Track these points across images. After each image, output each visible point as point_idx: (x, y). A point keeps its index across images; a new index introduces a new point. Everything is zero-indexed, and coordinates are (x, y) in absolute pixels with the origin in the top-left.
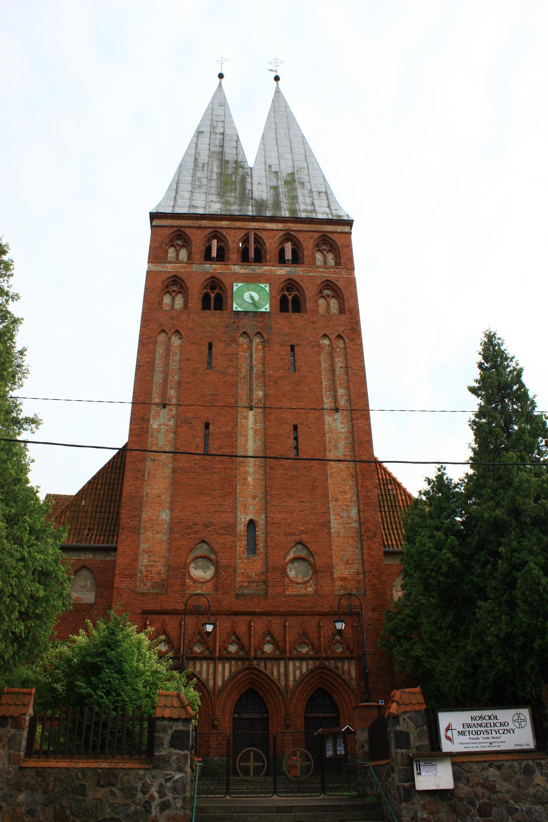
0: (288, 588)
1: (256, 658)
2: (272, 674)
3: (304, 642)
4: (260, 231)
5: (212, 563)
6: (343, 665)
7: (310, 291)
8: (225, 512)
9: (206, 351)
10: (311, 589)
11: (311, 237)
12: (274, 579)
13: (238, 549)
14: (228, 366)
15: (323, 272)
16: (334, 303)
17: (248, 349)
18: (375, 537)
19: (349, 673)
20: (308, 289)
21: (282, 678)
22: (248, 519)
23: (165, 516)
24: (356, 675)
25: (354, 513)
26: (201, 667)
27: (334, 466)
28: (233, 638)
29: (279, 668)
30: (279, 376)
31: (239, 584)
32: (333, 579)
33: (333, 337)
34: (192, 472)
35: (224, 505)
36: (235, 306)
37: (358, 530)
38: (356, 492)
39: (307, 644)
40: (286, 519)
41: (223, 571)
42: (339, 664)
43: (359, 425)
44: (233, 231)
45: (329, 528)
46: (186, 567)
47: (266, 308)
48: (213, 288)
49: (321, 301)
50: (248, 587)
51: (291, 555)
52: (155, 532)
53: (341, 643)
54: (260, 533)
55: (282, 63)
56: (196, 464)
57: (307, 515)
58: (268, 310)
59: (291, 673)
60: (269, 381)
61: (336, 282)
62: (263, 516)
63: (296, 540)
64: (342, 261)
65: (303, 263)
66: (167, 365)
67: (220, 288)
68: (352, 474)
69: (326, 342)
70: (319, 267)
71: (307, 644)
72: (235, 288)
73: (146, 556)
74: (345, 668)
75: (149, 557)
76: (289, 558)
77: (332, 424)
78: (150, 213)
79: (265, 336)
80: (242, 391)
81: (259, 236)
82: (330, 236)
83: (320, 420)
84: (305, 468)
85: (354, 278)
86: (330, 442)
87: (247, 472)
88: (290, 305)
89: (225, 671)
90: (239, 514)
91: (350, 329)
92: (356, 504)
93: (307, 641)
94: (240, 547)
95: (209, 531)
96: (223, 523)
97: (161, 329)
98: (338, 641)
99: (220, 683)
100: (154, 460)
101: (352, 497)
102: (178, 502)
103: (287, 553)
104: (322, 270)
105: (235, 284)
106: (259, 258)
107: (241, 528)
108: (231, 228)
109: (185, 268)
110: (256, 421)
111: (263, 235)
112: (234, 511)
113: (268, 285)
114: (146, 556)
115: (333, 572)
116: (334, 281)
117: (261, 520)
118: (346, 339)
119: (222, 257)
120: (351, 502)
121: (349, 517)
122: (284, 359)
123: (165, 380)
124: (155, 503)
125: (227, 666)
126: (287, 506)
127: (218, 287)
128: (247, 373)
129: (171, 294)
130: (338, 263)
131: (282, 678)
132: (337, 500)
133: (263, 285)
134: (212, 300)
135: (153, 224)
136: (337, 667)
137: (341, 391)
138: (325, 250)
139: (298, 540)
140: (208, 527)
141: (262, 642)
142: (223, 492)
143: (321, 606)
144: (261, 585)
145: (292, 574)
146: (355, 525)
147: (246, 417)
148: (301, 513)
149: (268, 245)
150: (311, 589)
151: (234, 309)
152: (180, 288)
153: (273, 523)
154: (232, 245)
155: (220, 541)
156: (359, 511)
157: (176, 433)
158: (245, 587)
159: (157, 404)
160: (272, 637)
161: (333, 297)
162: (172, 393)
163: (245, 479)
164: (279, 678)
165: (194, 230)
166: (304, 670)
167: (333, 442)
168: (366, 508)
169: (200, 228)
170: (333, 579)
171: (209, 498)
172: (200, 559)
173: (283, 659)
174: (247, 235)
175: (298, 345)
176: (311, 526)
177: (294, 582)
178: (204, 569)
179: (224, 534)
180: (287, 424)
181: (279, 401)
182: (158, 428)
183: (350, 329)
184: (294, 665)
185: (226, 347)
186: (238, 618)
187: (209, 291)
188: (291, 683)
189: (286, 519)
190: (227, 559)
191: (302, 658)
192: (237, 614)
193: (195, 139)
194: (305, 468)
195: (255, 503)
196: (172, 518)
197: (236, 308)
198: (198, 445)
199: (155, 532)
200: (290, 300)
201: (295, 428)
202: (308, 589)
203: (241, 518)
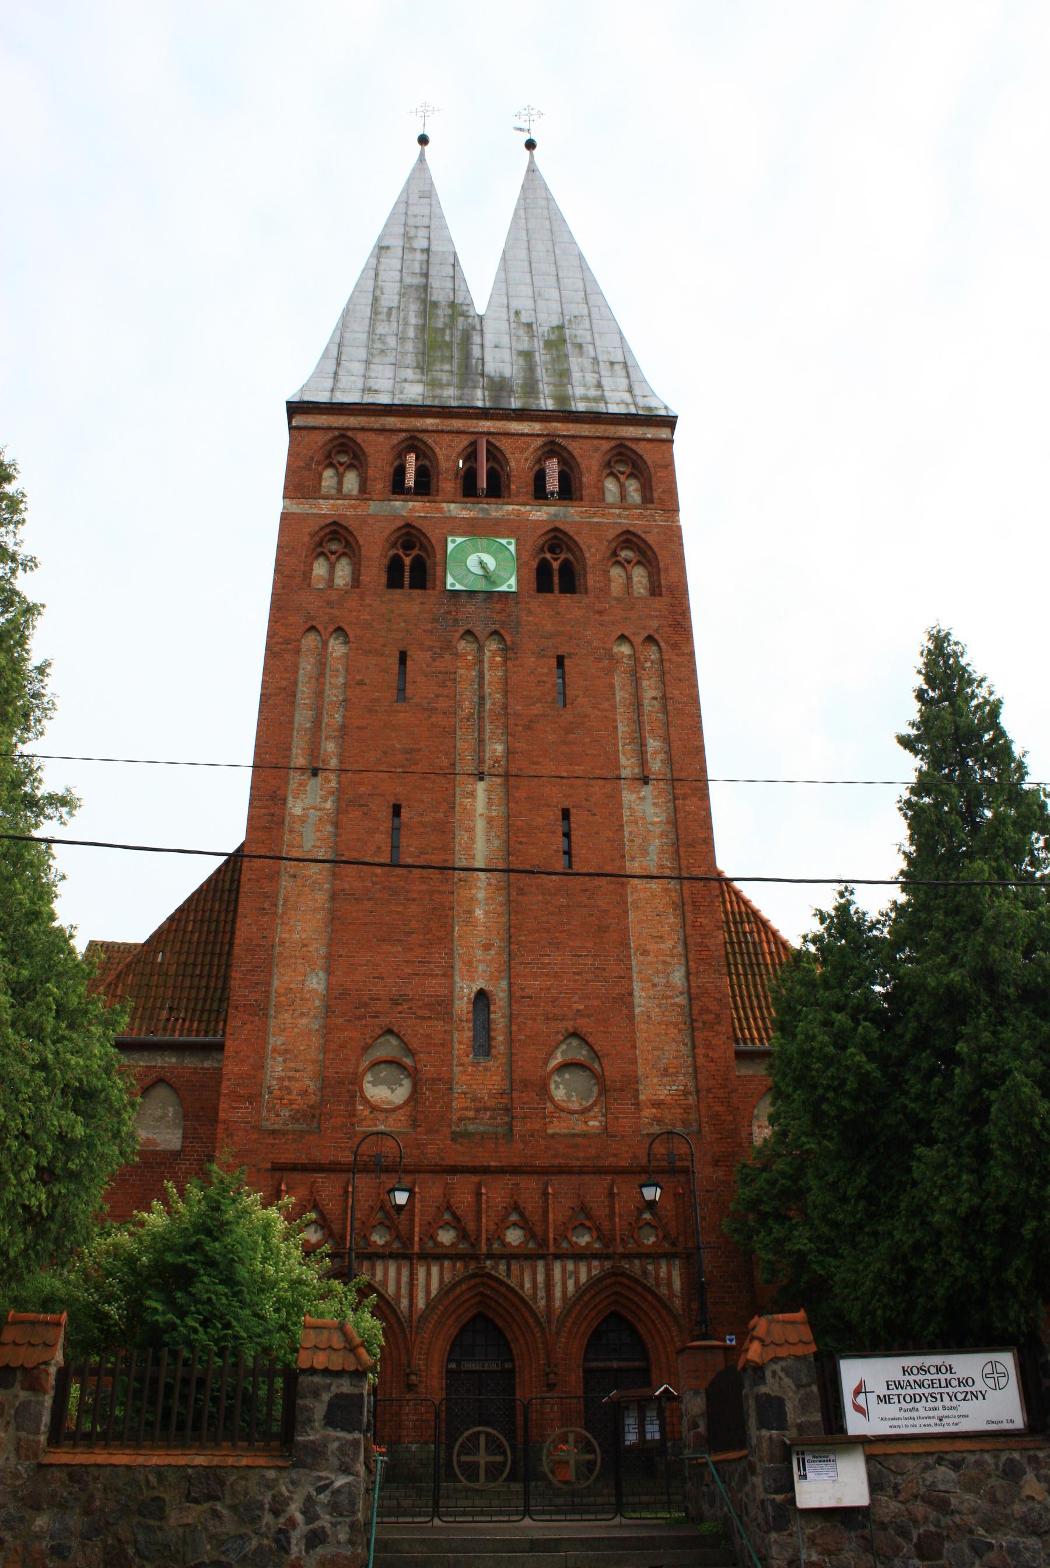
0: (552, 1122)
1: (490, 1256)
2: (522, 1286)
3: (582, 1225)
4: (498, 437)
5: (406, 1073)
6: (657, 1269)
7: (593, 552)
8: (431, 975)
9: (395, 668)
10: (597, 1124)
11: (596, 450)
12: (524, 1103)
13: (456, 1046)
14: (437, 696)
15: (619, 516)
18: (719, 1023)
19: (670, 1285)
20: (589, 547)
22: (474, 990)
23: (316, 983)
24: (682, 1289)
25: (678, 976)
28: (447, 1217)
29: (534, 1274)
31: (459, 1114)
36: (450, 580)
39: (589, 1228)
40: (548, 989)
41: (427, 1089)
42: (650, 1267)
43: (687, 808)
45: (631, 1006)
46: (357, 1081)
47: (510, 584)
48: (408, 546)
50: (475, 1119)
52: (297, 1013)
53: (654, 1227)
54: (498, 1015)
55: (541, 114)
57: (587, 981)
58: (514, 589)
60: (516, 725)
61: (643, 535)
62: (504, 984)
63: (567, 1030)
64: (655, 495)
65: (581, 499)
66: (319, 694)
67: (422, 547)
68: (674, 903)
70: (612, 506)
71: (589, 1228)
72: (450, 547)
73: (280, 1059)
75: (285, 1061)
76: (553, 1063)
77: (636, 808)
78: (288, 403)
79: (508, 638)
80: (464, 744)
81: (497, 448)
82: (634, 446)
83: (614, 799)
84: (586, 890)
85: (679, 528)
86: (632, 841)
87: (472, 899)
88: (556, 579)
89: (431, 1279)
90: (457, 979)
91: (670, 626)
92: (683, 961)
93: (588, 1223)
94: (460, 1043)
95: (400, 1013)
97: (309, 625)
99: (421, 1303)
100: (295, 876)
103: (550, 1055)
104: (617, 511)
105: (450, 539)
106: (497, 489)
107: (462, 1006)
111: (504, 444)
112: (448, 973)
113: (513, 541)
115: (637, 1090)
117: (500, 992)
118: (662, 644)
119: (425, 487)
120: (673, 956)
121: (668, 984)
123: (317, 722)
124: (296, 958)
126: (549, 964)
127: (418, 545)
128: (474, 708)
129: (327, 559)
130: (647, 499)
132: (645, 953)
133: (504, 541)
134: (407, 569)
136: (645, 1273)
138: (623, 473)
139: (571, 1030)
141: (503, 1225)
142: (427, 937)
143: (615, 1155)
145: (559, 1094)
146: (681, 1000)
147: (472, 794)
148: (577, 977)
150: (597, 1124)
151: (449, 587)
152: (345, 547)
153: (522, 997)
154: (444, 465)
155: (421, 1031)
157: (336, 825)
158: (469, 1119)
160: (522, 1215)
161: (639, 563)
162: (330, 747)
163: (470, 912)
164: (535, 1294)
165: (371, 436)
166: (583, 1278)
169: (382, 431)
170: (637, 1104)
171: (400, 949)
173: (542, 1257)
174: (474, 444)
175: (570, 655)
176: (596, 1003)
177: (563, 1110)
178: (391, 1084)
179: (430, 1018)
180: (549, 806)
181: (534, 763)
182: (303, 816)
183: (670, 626)
184: (564, 1269)
186: (456, 1178)
187: (401, 552)
188: (558, 1303)
189: (548, 989)
192: (453, 1170)
193: (374, 261)
194: (586, 890)
195: (490, 957)
196: (329, 987)
197: (453, 585)
199: (297, 1013)
200: (556, 568)
201: (566, 814)
202: (591, 1123)
203: (462, 988)
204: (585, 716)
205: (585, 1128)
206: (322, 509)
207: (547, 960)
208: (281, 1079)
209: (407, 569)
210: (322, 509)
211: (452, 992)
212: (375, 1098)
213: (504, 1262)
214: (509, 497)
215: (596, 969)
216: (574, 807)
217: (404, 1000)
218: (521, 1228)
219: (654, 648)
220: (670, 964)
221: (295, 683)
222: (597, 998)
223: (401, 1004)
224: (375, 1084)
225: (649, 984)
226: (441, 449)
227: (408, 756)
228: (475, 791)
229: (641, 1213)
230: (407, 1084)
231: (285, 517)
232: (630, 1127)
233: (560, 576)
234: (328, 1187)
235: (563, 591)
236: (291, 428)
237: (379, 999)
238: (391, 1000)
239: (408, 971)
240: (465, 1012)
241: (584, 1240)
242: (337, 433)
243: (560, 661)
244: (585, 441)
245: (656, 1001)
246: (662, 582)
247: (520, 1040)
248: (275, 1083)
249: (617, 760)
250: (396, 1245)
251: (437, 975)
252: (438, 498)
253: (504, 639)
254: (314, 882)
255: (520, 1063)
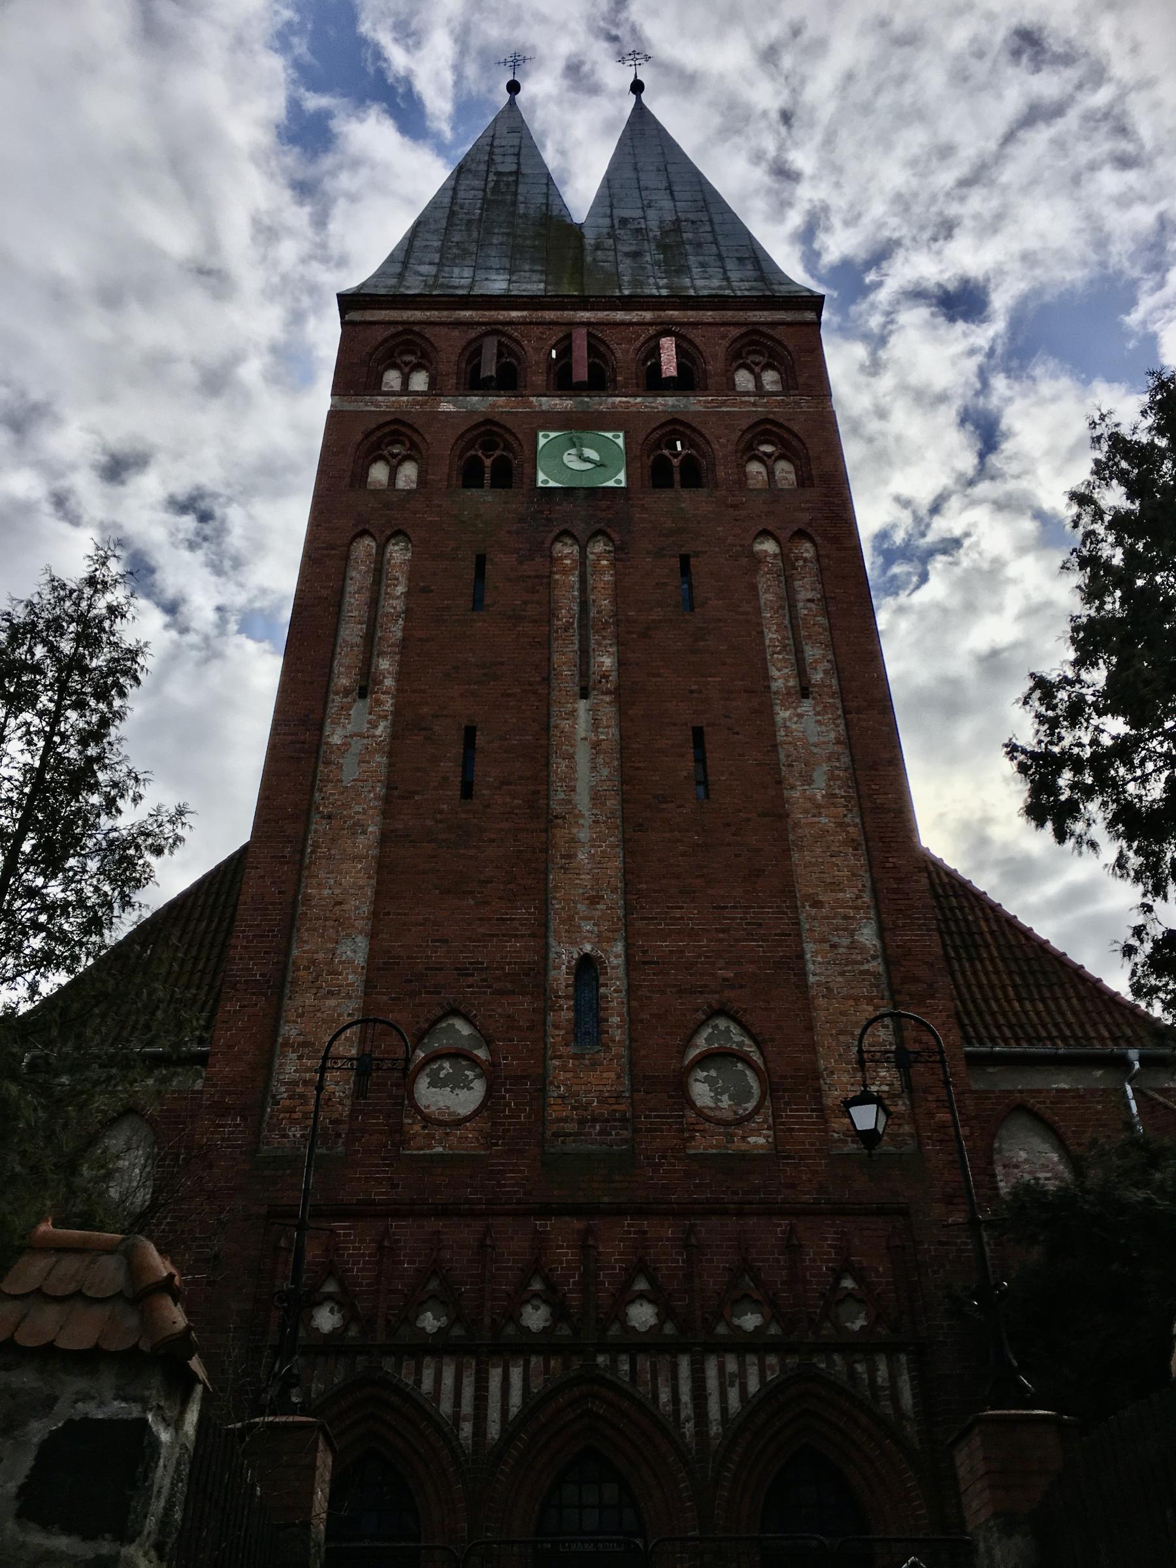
0: (693, 1138)
1: (602, 1348)
2: (656, 1397)
3: (747, 1297)
4: (600, 328)
5: (478, 1070)
6: (872, 1371)
7: (722, 445)
8: (516, 936)
9: (470, 575)
10: (762, 1141)
11: (723, 337)
12: (651, 1110)
13: (551, 1030)
14: (525, 603)
15: (754, 404)
16: (785, 471)
17: (575, 568)
18: (932, 997)
19: (895, 1398)
20: (718, 438)
21: (687, 1411)
22: (576, 956)
23: (355, 951)
24: (915, 1405)
25: (867, 936)
26: (438, 1380)
27: (803, 821)
28: (537, 1286)
29: (675, 1377)
30: (653, 621)
31: (554, 1128)
32: (821, 1110)
33: (785, 535)
34: (429, 842)
35: (512, 919)
36: (541, 476)
37: (884, 979)
38: (868, 884)
39: (756, 1302)
40: (682, 952)
41: (507, 1091)
42: (860, 1368)
43: (864, 724)
44: (537, 330)
45: (803, 974)
46: (407, 1080)
47: (619, 479)
48: (488, 447)
49: (755, 468)
50: (579, 1134)
51: (701, 1044)
52: (322, 992)
53: (860, 1301)
54: (614, 988)
56: (441, 821)
57: (737, 940)
58: (623, 485)
59: (717, 1392)
60: (629, 633)
61: (786, 423)
62: (619, 948)
63: (710, 1006)
64: (801, 380)
65: (706, 388)
66: (374, 603)
67: (508, 447)
68: (853, 840)
69: (769, 547)
70: (747, 394)
71: (756, 1302)
72: (542, 441)
73: (294, 1056)
74: (880, 1380)
75: (300, 1058)
76: (693, 1053)
77: (794, 726)
78: (338, 295)
79: (614, 536)
80: (564, 658)
81: (600, 340)
82: (770, 331)
83: (765, 712)
84: (728, 825)
85: (833, 414)
86: (791, 766)
87: (573, 840)
88: (677, 477)
89: (510, 1386)
90: (552, 942)
91: (827, 518)
92: (872, 913)
93: (756, 1295)
94: (557, 1027)
95: (469, 987)
96: (509, 964)
97: (360, 528)
98: (850, 1295)
99: (494, 1430)
100: (329, 817)
101: (858, 897)
102: (388, 914)
103: (688, 1042)
104: (752, 399)
105: (541, 434)
106: (599, 382)
107: (561, 977)
108: (531, 323)
109: (422, 404)
110: (596, 724)
111: (606, 335)
112: (541, 932)
113: (621, 434)
114: (294, 1056)
115: (819, 1090)
116: (781, 421)
117: (615, 956)
118: (818, 539)
119: (508, 380)
120: (857, 908)
121: (853, 945)
122: (665, 584)
123: (369, 639)
124: (326, 919)
125: (516, 1375)
126: (682, 918)
127: (502, 445)
128: (573, 617)
129: (388, 462)
130: (789, 384)
131: (687, 1411)
132: (817, 904)
133: (609, 435)
134: (488, 470)
135: (347, 317)
136: (852, 1375)
137: (812, 652)
138: (757, 364)
139: (716, 1006)
140: (468, 975)
141: (624, 1297)
142: (510, 886)
143: (792, 1186)
144: (615, 1128)
145: (701, 1092)
146: (876, 966)
147: (573, 714)
148: (721, 935)
149: (619, 354)
150: (762, 1141)
151: (540, 484)
152: (409, 449)
153: (644, 963)
154: (533, 357)
155: (500, 1010)
156: (881, 932)
157: (390, 755)
158: (570, 1135)
159: (347, 692)
160: (652, 1281)
161: (782, 457)
162: (384, 664)
163: (570, 856)
164: (676, 1412)
165: (444, 330)
166: (753, 1386)
167: (799, 766)
168: (900, 922)
169: (458, 324)
170: (821, 1110)
171: (472, 902)
172: (1021, 134)
173: (684, 1349)
174: (568, 336)
175: (697, 554)
176: (751, 968)
177: (708, 1119)
178: (457, 1082)
179: (513, 992)
180: (675, 724)
181: (654, 675)
182: (344, 744)
183: (827, 518)
184: (721, 1368)
185: (521, 563)
186: (550, 1224)
187: (480, 453)
188: (715, 1429)
189: (682, 952)
190: (519, 1059)
191: (744, 1345)
192: (545, 1211)
193: (453, 182)
194: (728, 825)
195: (598, 913)
196: (372, 956)
197: (546, 482)
198: (445, 779)
199: (322, 992)
201: (698, 735)
202: (751, 1140)
203: (559, 954)
204: (720, 620)
205: (743, 1146)
206: (381, 406)
207: (677, 913)
208: (295, 1083)
209: (488, 470)
210: (381, 406)
211: (546, 958)
212: (433, 1108)
213: (624, 1357)
214: (615, 389)
215: (748, 924)
216: (708, 725)
217: (475, 969)
218: (650, 1301)
219: (808, 545)
220: (853, 918)
221: (341, 592)
222: (752, 963)
223: (472, 975)
224: (435, 1083)
225: (826, 946)
226: (529, 341)
227: (486, 671)
228: (575, 710)
229: (838, 1280)
230: (479, 1088)
231: (333, 416)
232: (812, 1144)
233: (681, 473)
234: (353, 1242)
235: (684, 485)
236: (343, 324)
237: (441, 969)
238: (457, 969)
239: (482, 930)
240: (563, 987)
241: (750, 1321)
242: (400, 328)
243: (685, 560)
244: (710, 328)
245: (838, 968)
246: (814, 472)
247: (642, 1021)
248: (283, 1089)
249: (766, 669)
250: (458, 1331)
251: (523, 936)
252: (527, 392)
253: (612, 540)
254: (355, 824)
255: (643, 1052)
